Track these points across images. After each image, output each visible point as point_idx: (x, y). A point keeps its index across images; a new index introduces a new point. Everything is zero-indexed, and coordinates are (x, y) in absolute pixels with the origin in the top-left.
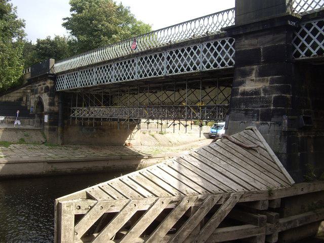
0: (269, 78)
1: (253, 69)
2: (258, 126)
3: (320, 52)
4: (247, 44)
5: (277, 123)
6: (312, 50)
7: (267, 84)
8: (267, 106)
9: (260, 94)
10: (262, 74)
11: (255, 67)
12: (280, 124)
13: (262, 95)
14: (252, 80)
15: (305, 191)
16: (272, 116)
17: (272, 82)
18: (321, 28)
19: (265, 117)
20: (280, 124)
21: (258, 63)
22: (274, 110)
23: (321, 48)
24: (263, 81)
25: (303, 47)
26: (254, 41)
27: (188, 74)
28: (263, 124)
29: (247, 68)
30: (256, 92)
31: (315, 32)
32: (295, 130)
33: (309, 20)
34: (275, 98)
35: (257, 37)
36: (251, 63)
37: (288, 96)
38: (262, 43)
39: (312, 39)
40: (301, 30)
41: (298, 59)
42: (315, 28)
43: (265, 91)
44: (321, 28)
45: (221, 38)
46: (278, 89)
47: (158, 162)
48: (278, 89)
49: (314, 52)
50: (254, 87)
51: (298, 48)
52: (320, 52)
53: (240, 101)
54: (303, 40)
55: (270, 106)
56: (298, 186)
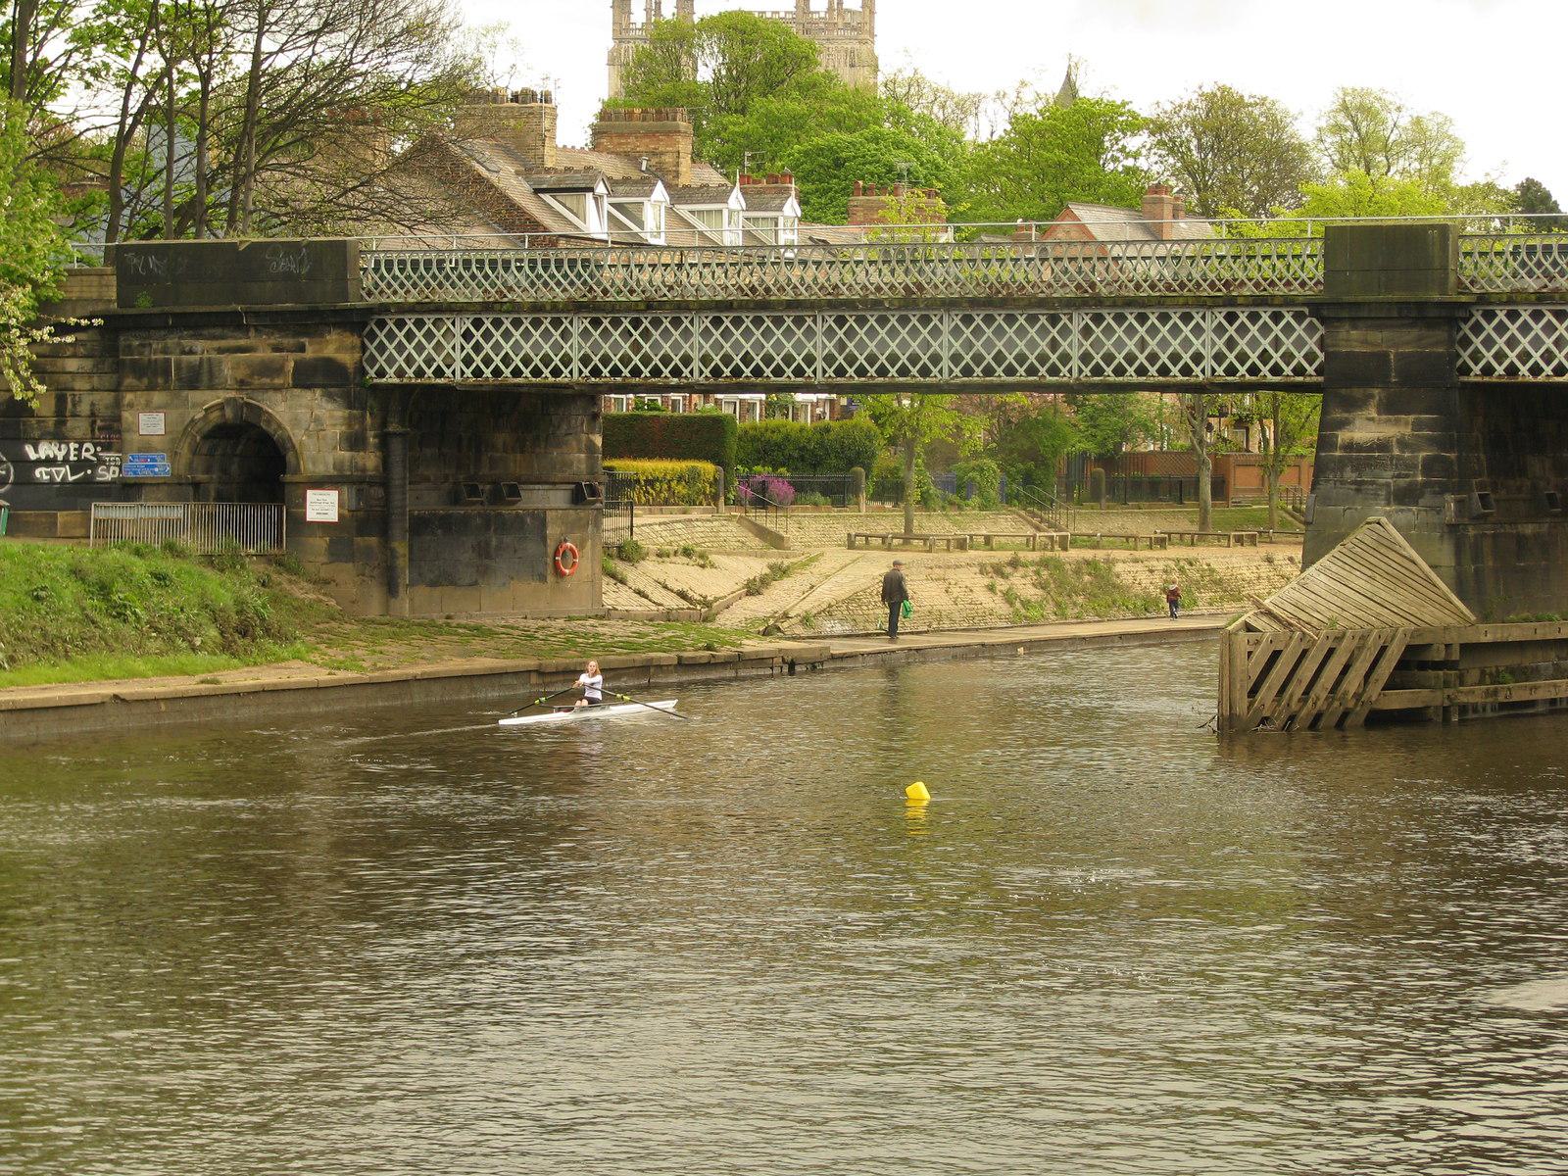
0: (1411, 418)
1: (1372, 396)
2: (1388, 515)
3: (1560, 370)
4: (1354, 340)
5: (1432, 508)
6: (1495, 364)
7: (1408, 431)
8: (1407, 476)
9: (1391, 451)
10: (1391, 408)
11: (1376, 391)
12: (1438, 510)
13: (1396, 452)
14: (1369, 419)
15: (1489, 638)
16: (1422, 495)
17: (1417, 426)
18: (1561, 322)
19: (1405, 496)
20: (1438, 510)
21: (1385, 384)
22: (1425, 485)
23: (1560, 363)
24: (1397, 422)
25: (1476, 357)
26: (1376, 336)
27: (416, 385)
28: (1402, 511)
29: (1357, 392)
30: (1382, 446)
31: (1549, 329)
32: (1466, 521)
33: (1491, 303)
34: (1426, 460)
35: (1380, 328)
36: (1368, 382)
37: (1453, 456)
38: (1397, 343)
39: (1495, 343)
40: (1473, 320)
41: (1465, 379)
42: (1501, 321)
43: (1403, 444)
44: (1561, 322)
45: (754, 309)
46: (1431, 441)
47: (814, 581)
48: (1431, 441)
49: (1500, 370)
50: (1377, 435)
51: (1465, 355)
52: (1560, 370)
53: (1341, 464)
54: (1477, 342)
55: (1415, 475)
56: (1483, 627)
